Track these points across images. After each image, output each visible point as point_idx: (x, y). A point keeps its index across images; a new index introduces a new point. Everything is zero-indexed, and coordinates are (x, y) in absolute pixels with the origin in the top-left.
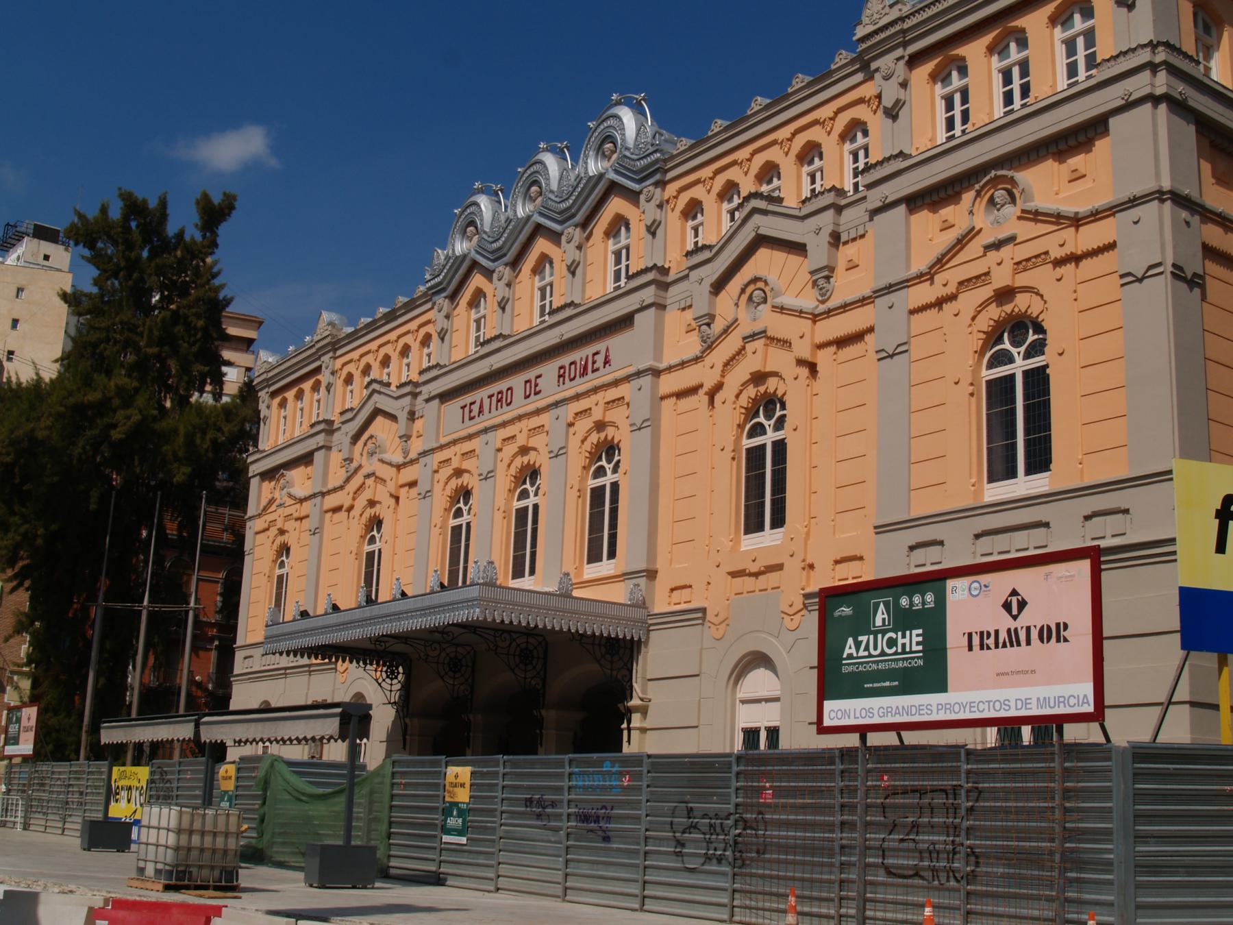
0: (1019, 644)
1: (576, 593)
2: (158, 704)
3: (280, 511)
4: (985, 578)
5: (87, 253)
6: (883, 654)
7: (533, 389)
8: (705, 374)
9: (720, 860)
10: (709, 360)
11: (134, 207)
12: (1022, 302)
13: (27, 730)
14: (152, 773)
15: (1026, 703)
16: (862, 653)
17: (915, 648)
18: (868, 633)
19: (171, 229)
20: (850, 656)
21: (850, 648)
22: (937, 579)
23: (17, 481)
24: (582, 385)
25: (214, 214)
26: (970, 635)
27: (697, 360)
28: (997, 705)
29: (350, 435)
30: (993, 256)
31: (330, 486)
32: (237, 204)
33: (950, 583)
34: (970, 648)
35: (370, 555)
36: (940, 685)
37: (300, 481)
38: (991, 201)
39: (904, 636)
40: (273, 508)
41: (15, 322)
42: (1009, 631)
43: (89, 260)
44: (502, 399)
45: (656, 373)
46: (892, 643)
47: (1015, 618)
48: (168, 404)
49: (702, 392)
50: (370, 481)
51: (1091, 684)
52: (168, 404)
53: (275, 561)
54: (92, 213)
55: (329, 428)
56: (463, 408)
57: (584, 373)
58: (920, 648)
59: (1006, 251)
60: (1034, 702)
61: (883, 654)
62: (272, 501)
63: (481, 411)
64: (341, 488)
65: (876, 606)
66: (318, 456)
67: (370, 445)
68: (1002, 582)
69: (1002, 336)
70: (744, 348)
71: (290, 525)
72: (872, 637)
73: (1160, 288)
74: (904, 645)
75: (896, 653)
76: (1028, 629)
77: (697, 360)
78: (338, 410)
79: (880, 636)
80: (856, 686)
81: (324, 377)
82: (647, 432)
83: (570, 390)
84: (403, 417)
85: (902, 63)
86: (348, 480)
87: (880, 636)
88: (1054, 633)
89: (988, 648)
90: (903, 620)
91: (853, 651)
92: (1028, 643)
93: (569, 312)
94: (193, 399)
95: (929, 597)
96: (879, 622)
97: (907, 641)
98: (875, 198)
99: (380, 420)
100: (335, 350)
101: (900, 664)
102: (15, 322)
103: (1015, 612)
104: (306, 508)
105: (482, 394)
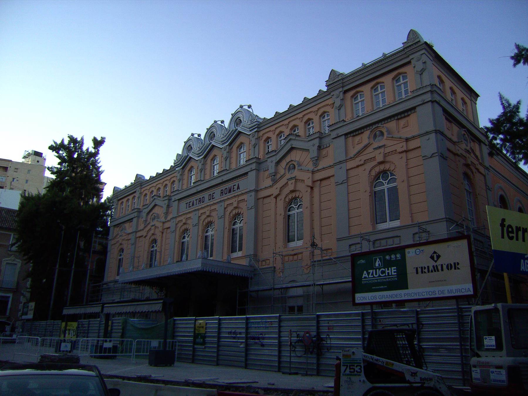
0: (438, 271)
1: (232, 262)
2: (77, 301)
3: (121, 238)
4: (422, 248)
5: (57, 154)
6: (379, 276)
7: (211, 197)
8: (144, 233)
9: (311, 353)
10: (275, 187)
11: (73, 140)
12: (387, 166)
13: (31, 310)
14: (78, 325)
15: (443, 292)
16: (370, 276)
17: (393, 274)
18: (373, 269)
19: (84, 148)
20: (365, 277)
21: (365, 274)
22: (402, 249)
23: (83, 196)
24: (229, 195)
25: (98, 143)
26: (417, 268)
27: (271, 186)
28: (430, 293)
29: (274, 162)
31: (139, 229)
32: (106, 140)
33: (407, 250)
34: (417, 273)
35: (120, 259)
36: (405, 286)
37: (129, 228)
38: (375, 134)
39: (388, 270)
40: (118, 236)
41: (27, 181)
42: (433, 266)
43: (57, 157)
44: (201, 201)
45: (136, 232)
46: (383, 272)
47: (436, 261)
48: (82, 204)
49: (272, 197)
50: (153, 227)
51: (471, 284)
52: (82, 204)
53: (150, 246)
54: (59, 142)
55: (139, 211)
56: (187, 204)
57: (230, 191)
58: (396, 274)
59: (382, 150)
60: (446, 292)
61: (379, 276)
62: (118, 234)
63: (193, 205)
64: (143, 230)
65: (376, 260)
66: (135, 220)
67: (153, 216)
68: (430, 249)
69: (379, 177)
70: (287, 182)
71: (124, 242)
72: (374, 271)
73: (436, 161)
74: (388, 273)
75: (385, 276)
76: (442, 265)
77: (271, 186)
78: (142, 205)
79: (378, 270)
80: (369, 288)
81: (137, 195)
82: (174, 233)
83: (225, 197)
84: (165, 207)
85: (341, 93)
86: (145, 227)
87: (378, 270)
88: (455, 266)
89: (425, 273)
90: (387, 264)
91: (367, 276)
92: (442, 270)
93: (177, 192)
94: (90, 203)
95: (398, 256)
96: (377, 265)
97: (390, 271)
98: (334, 134)
99: (156, 208)
100: (141, 186)
101: (387, 280)
102: (27, 181)
103: (435, 259)
104: (131, 236)
105: (193, 199)
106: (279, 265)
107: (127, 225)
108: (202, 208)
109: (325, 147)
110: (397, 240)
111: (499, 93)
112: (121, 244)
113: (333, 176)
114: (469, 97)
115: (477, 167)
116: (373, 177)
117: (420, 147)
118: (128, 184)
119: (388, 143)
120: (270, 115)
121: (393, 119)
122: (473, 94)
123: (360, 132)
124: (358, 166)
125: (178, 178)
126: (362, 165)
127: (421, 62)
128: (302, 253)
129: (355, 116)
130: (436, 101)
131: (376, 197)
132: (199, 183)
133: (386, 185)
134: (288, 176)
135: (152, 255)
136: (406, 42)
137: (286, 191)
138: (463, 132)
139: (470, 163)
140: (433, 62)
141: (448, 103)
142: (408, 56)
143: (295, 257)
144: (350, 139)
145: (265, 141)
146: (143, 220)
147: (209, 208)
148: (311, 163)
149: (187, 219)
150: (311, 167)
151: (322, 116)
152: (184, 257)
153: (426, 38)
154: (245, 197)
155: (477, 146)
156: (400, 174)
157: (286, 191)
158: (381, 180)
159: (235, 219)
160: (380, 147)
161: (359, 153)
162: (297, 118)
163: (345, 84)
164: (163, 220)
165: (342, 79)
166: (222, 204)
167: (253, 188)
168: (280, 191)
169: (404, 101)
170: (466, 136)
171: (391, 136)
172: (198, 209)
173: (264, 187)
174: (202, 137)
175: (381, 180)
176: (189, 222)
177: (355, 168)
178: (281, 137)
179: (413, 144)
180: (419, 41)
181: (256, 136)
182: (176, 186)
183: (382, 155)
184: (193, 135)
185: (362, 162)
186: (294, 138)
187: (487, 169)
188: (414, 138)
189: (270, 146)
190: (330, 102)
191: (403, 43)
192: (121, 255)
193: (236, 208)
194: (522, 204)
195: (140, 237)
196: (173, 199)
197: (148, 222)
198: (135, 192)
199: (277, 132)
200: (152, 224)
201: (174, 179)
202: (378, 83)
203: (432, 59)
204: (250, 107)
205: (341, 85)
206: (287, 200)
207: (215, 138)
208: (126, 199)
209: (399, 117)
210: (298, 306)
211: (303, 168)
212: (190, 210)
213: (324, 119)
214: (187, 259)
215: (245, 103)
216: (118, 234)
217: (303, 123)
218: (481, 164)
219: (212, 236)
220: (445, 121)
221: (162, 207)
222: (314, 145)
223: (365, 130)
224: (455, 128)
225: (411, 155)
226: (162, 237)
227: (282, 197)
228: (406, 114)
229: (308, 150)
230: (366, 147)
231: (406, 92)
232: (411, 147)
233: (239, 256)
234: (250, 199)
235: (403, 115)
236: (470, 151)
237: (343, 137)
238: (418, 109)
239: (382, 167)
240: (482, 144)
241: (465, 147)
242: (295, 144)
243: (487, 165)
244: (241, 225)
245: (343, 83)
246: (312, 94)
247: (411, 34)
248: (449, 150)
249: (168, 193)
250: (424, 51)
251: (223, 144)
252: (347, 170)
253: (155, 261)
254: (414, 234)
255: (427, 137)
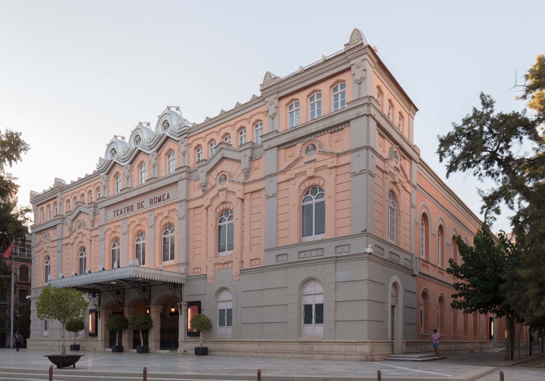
3: (45, 245)
7: (140, 206)
8: (70, 240)
10: (206, 198)
12: (316, 181)
24: (159, 205)
27: (202, 197)
29: (205, 172)
30: (309, 166)
40: (42, 244)
44: (130, 209)
45: (187, 201)
49: (203, 208)
55: (63, 218)
57: (160, 200)
59: (313, 164)
62: (41, 242)
63: (121, 213)
64: (69, 237)
66: (59, 227)
67: (79, 223)
69: (308, 192)
71: (49, 250)
77: (202, 197)
78: (65, 211)
81: (58, 200)
84: (91, 214)
85: (276, 100)
98: (266, 146)
99: (82, 215)
105: (121, 207)
106: (210, 273)
107: (51, 232)
108: (131, 217)
109: (257, 158)
110: (346, 249)
111: (482, 95)
112: (114, 232)
113: (264, 189)
114: (408, 112)
115: (404, 185)
116: (302, 191)
117: (350, 163)
118: (47, 188)
119: (319, 157)
120: (200, 121)
121: (326, 132)
122: (412, 108)
123: (292, 144)
124: (288, 180)
125: (103, 184)
126: (293, 179)
127: (361, 69)
128: (232, 262)
129: (140, 184)
130: (371, 115)
131: (306, 211)
132: (127, 191)
133: (314, 200)
134: (219, 187)
135: (82, 262)
136: (348, 44)
137: (217, 202)
138: (395, 149)
139: (397, 181)
140: (375, 70)
141: (384, 117)
142: (349, 62)
143: (226, 266)
144: (282, 152)
145: (195, 148)
146: (67, 227)
147: (138, 217)
148: (242, 175)
149: (141, 220)
150: (242, 179)
151: (255, 124)
152: (116, 265)
153: (369, 40)
154: (175, 207)
155: (408, 163)
156: (329, 190)
157: (217, 202)
158: (310, 195)
159: (166, 229)
160: (311, 162)
161: (290, 167)
162: (214, 132)
163: (280, 89)
164: (90, 227)
165: (278, 83)
166: (126, 221)
167: (184, 198)
168: (211, 202)
169: (289, 132)
170: (398, 153)
171: (323, 150)
172: (127, 218)
173: (195, 197)
174: (127, 140)
175: (310, 195)
176: (118, 230)
177: (285, 181)
178: (212, 145)
179: (344, 160)
180: (362, 44)
181: (185, 143)
182: (102, 193)
183: (313, 169)
184: (116, 137)
185: (293, 176)
186: (225, 147)
187: (414, 187)
188: (344, 153)
189: (243, 138)
190: (263, 109)
191: (345, 45)
192: (47, 262)
193: (166, 217)
194: (443, 221)
195: (66, 244)
196: (99, 206)
197: (73, 230)
198: (56, 197)
199: (238, 126)
200: (78, 231)
201: (99, 185)
202: (293, 100)
203: (373, 66)
204: (178, 109)
205: (276, 90)
206: (218, 211)
207: (141, 142)
208: (46, 204)
209: (333, 130)
210: (228, 310)
211: (234, 179)
212: (119, 219)
213: (257, 129)
214: (119, 267)
215: (173, 103)
216: (41, 242)
217: (95, 190)
218: (408, 182)
219: (144, 244)
220: (378, 136)
221: (88, 214)
222: (245, 156)
223: (298, 142)
224: (388, 145)
225: (341, 171)
226: (91, 244)
227: (213, 208)
228: (340, 128)
229: (239, 161)
230: (297, 161)
231: (343, 102)
232: (341, 163)
233: (171, 264)
234: (181, 209)
235: (336, 129)
236: (400, 169)
237: (276, 148)
238: (352, 123)
239: (312, 182)
240: (413, 161)
241: (395, 165)
242: (227, 154)
243: (414, 183)
244: (172, 234)
245: (278, 88)
246: (245, 99)
247: (355, 34)
248: (377, 167)
249: (94, 200)
250: (366, 56)
251: (180, 136)
252: (278, 183)
253: (85, 268)
254: (251, 260)
255: (357, 153)
